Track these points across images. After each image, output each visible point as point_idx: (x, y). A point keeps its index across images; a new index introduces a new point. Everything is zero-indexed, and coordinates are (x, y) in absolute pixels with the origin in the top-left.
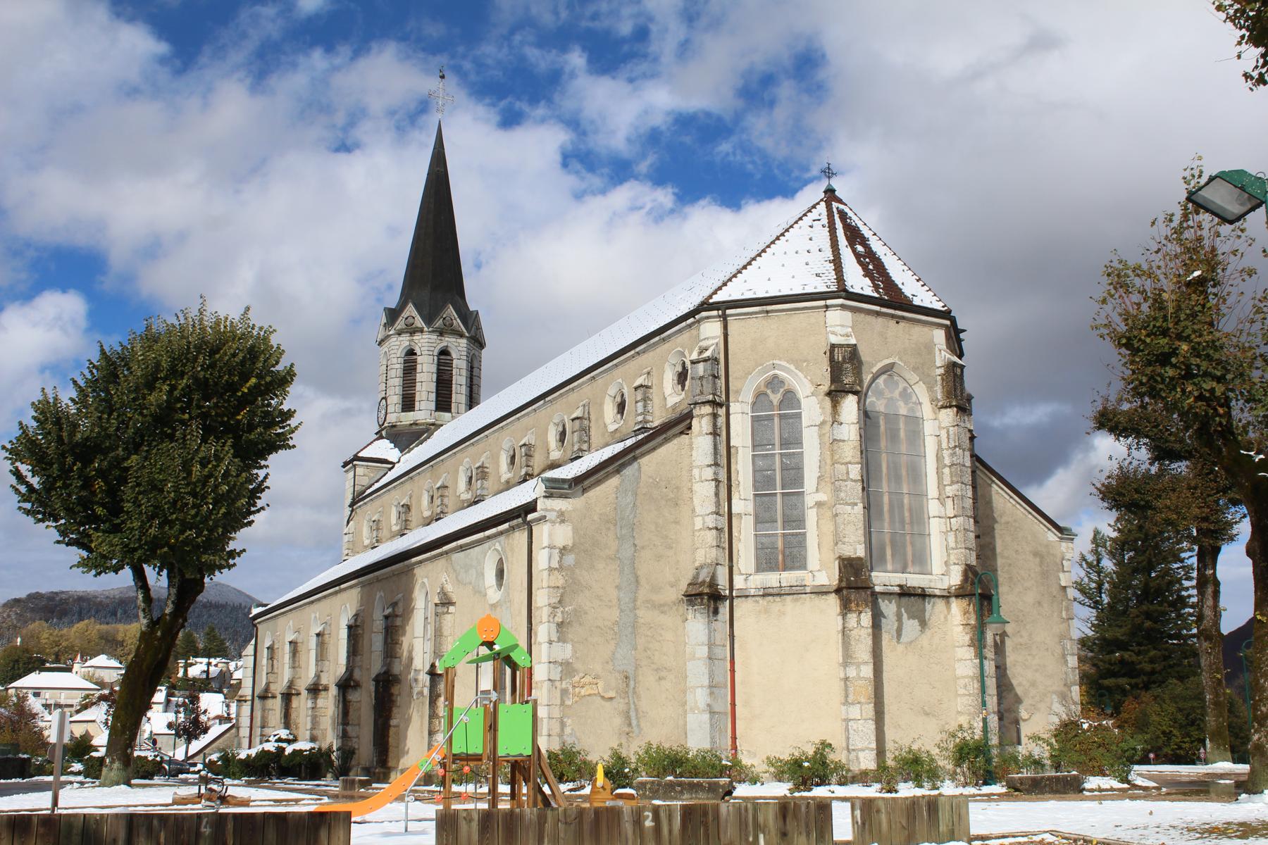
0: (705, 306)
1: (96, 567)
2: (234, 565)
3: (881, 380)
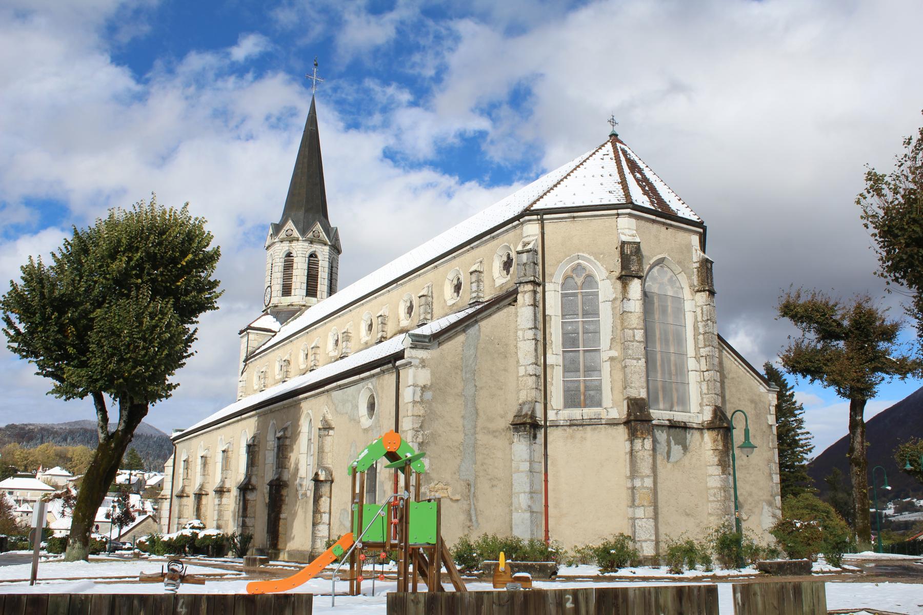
0: (527, 212)
1: (66, 393)
2: (171, 395)
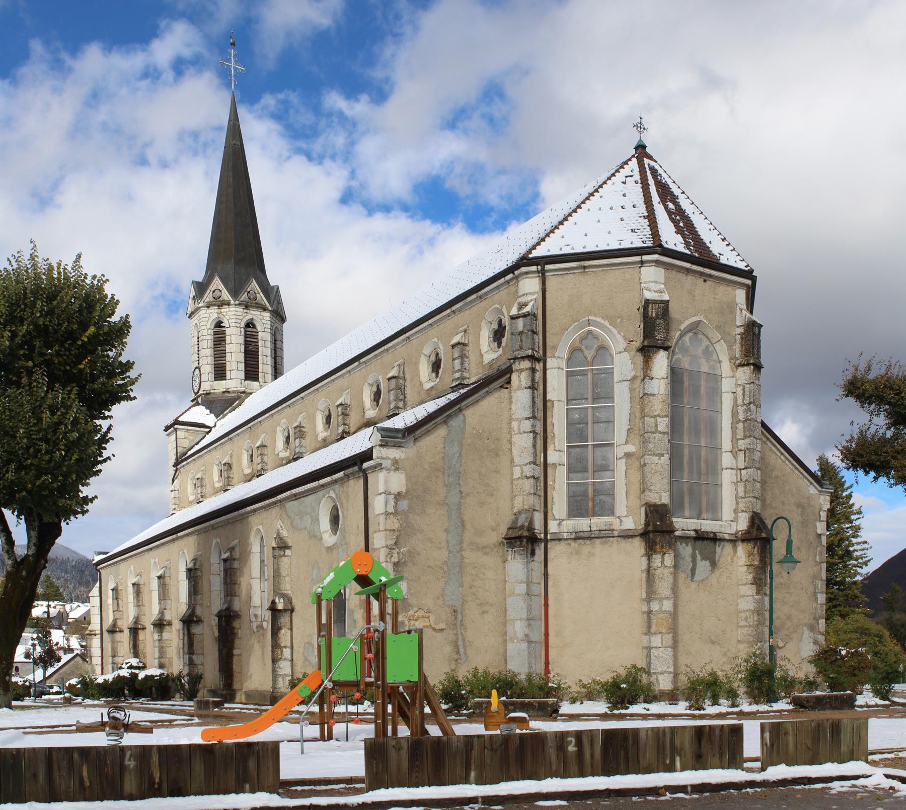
0: (525, 261)
2: (87, 511)
3: (687, 338)
